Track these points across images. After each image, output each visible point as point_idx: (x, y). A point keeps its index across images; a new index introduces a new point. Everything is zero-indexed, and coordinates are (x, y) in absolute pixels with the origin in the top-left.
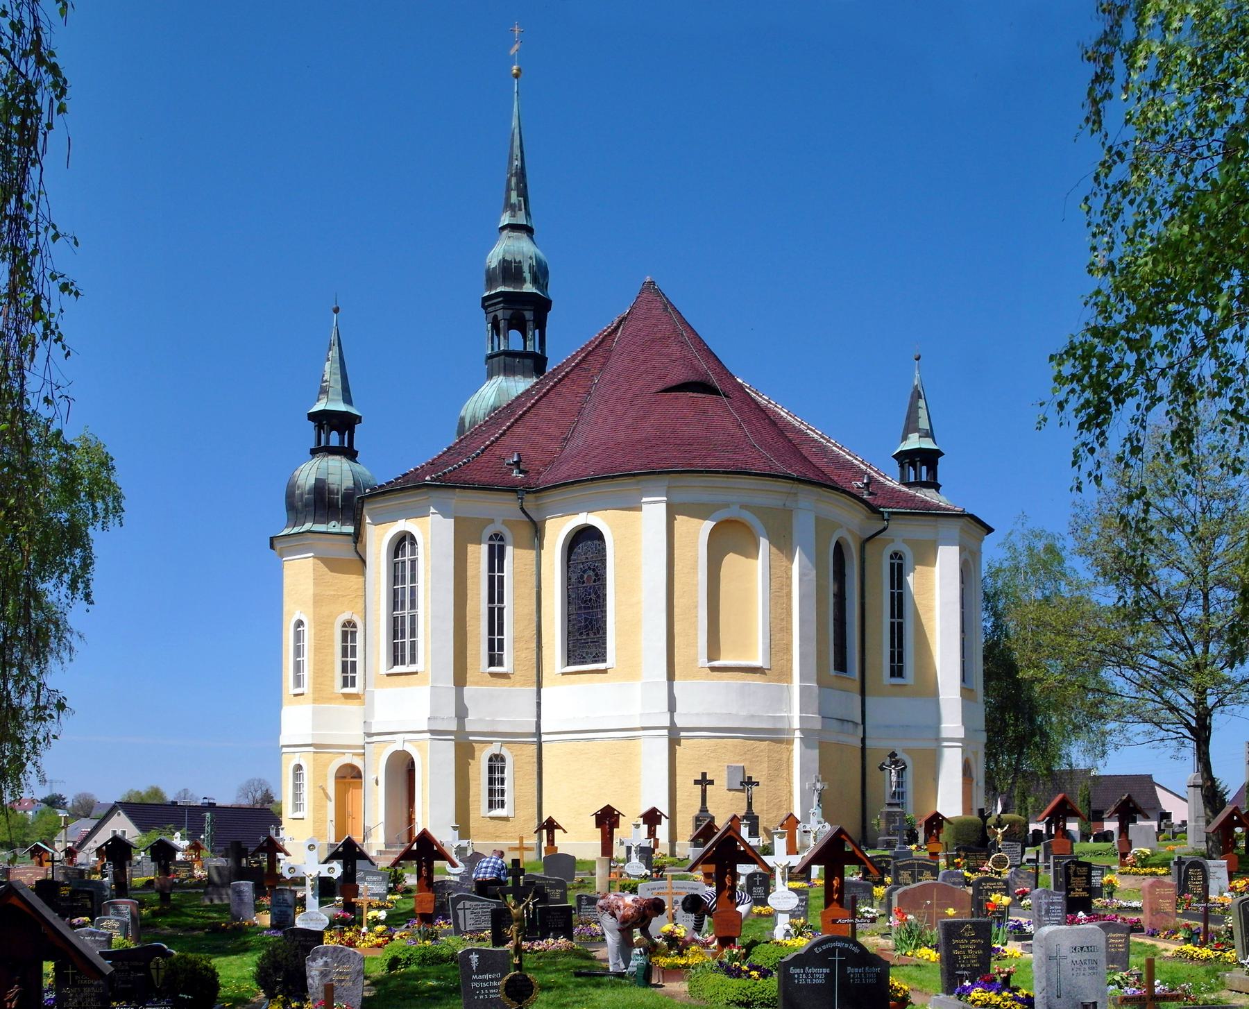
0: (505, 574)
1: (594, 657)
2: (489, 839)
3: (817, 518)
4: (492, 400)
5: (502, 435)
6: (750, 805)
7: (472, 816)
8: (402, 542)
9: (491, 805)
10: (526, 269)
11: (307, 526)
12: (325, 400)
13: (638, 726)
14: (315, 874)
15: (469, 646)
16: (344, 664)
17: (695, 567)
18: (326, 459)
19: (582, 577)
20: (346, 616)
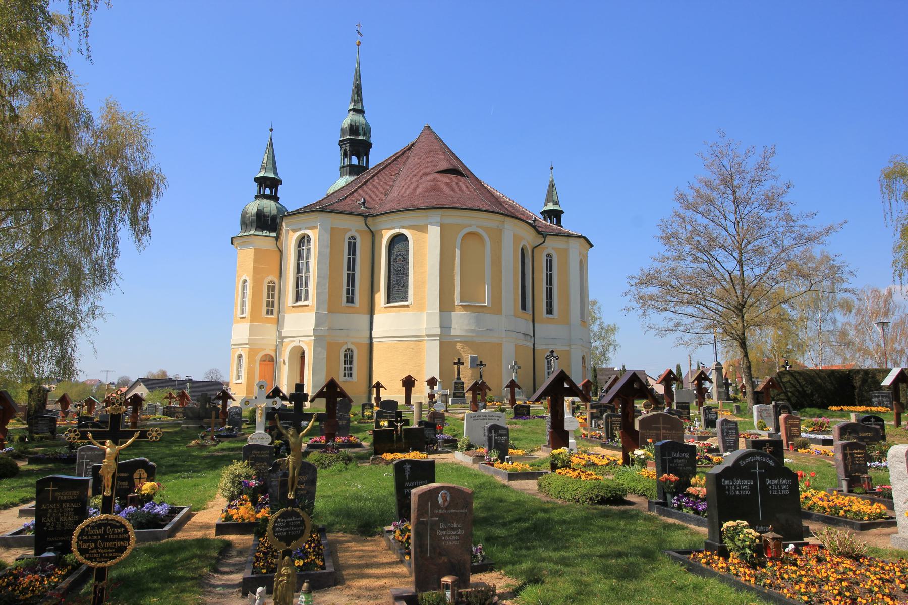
3: (514, 235)
8: (303, 241)
11: (252, 232)
16: (268, 302)
19: (396, 259)
20: (270, 278)
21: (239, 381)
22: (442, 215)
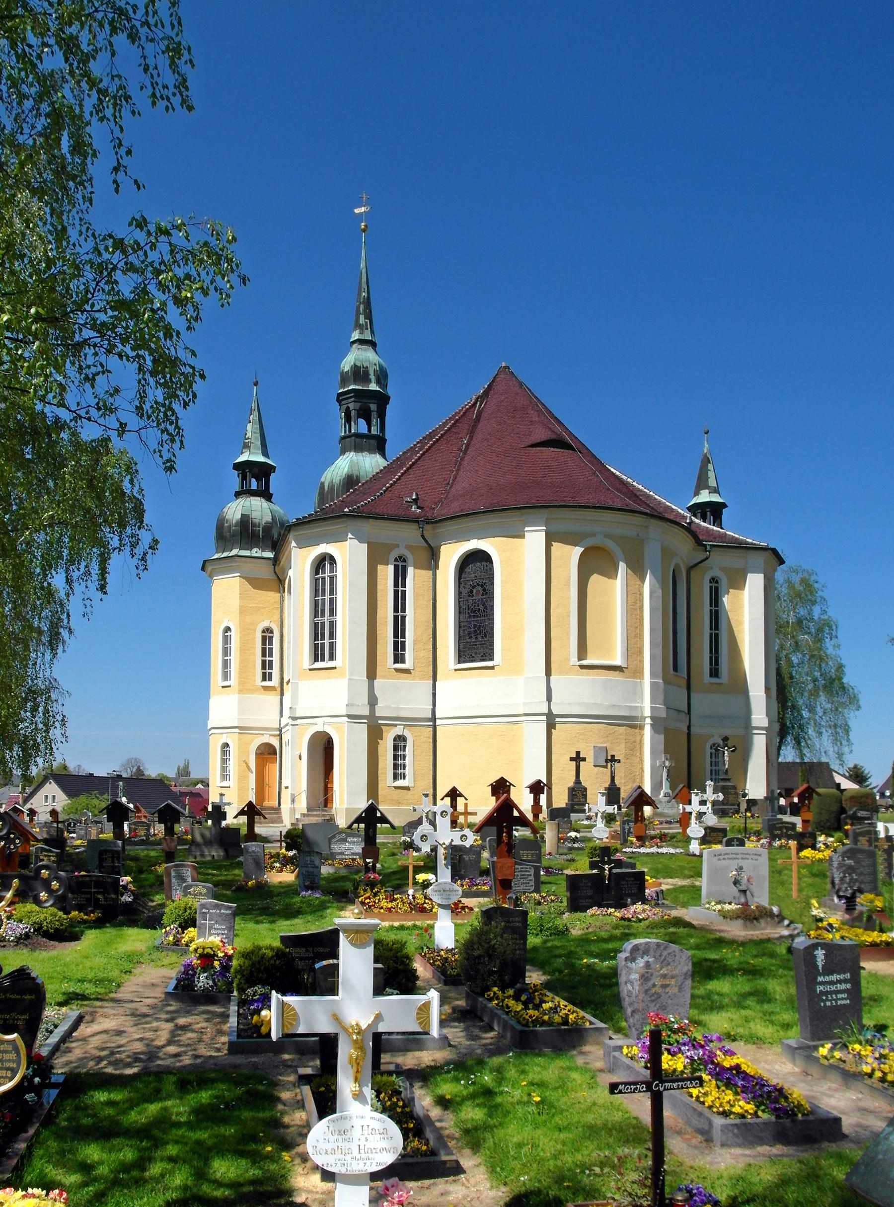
0: (407, 589)
2: (393, 805)
3: (662, 548)
4: (346, 470)
5: (398, 480)
6: (613, 778)
7: (381, 785)
8: (323, 562)
9: (396, 777)
10: (371, 372)
11: (235, 552)
13: (522, 712)
14: (447, 842)
15: (378, 647)
16: (264, 662)
17: (568, 584)
19: (471, 591)
20: (266, 624)
21: (225, 784)
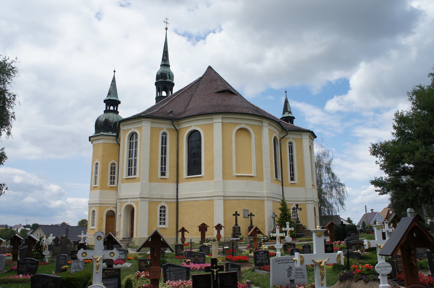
1: (197, 173)
6: (251, 223)
11: (101, 133)
12: (110, 96)
16: (111, 177)
18: (109, 113)
20: (113, 161)
22: (222, 118)
